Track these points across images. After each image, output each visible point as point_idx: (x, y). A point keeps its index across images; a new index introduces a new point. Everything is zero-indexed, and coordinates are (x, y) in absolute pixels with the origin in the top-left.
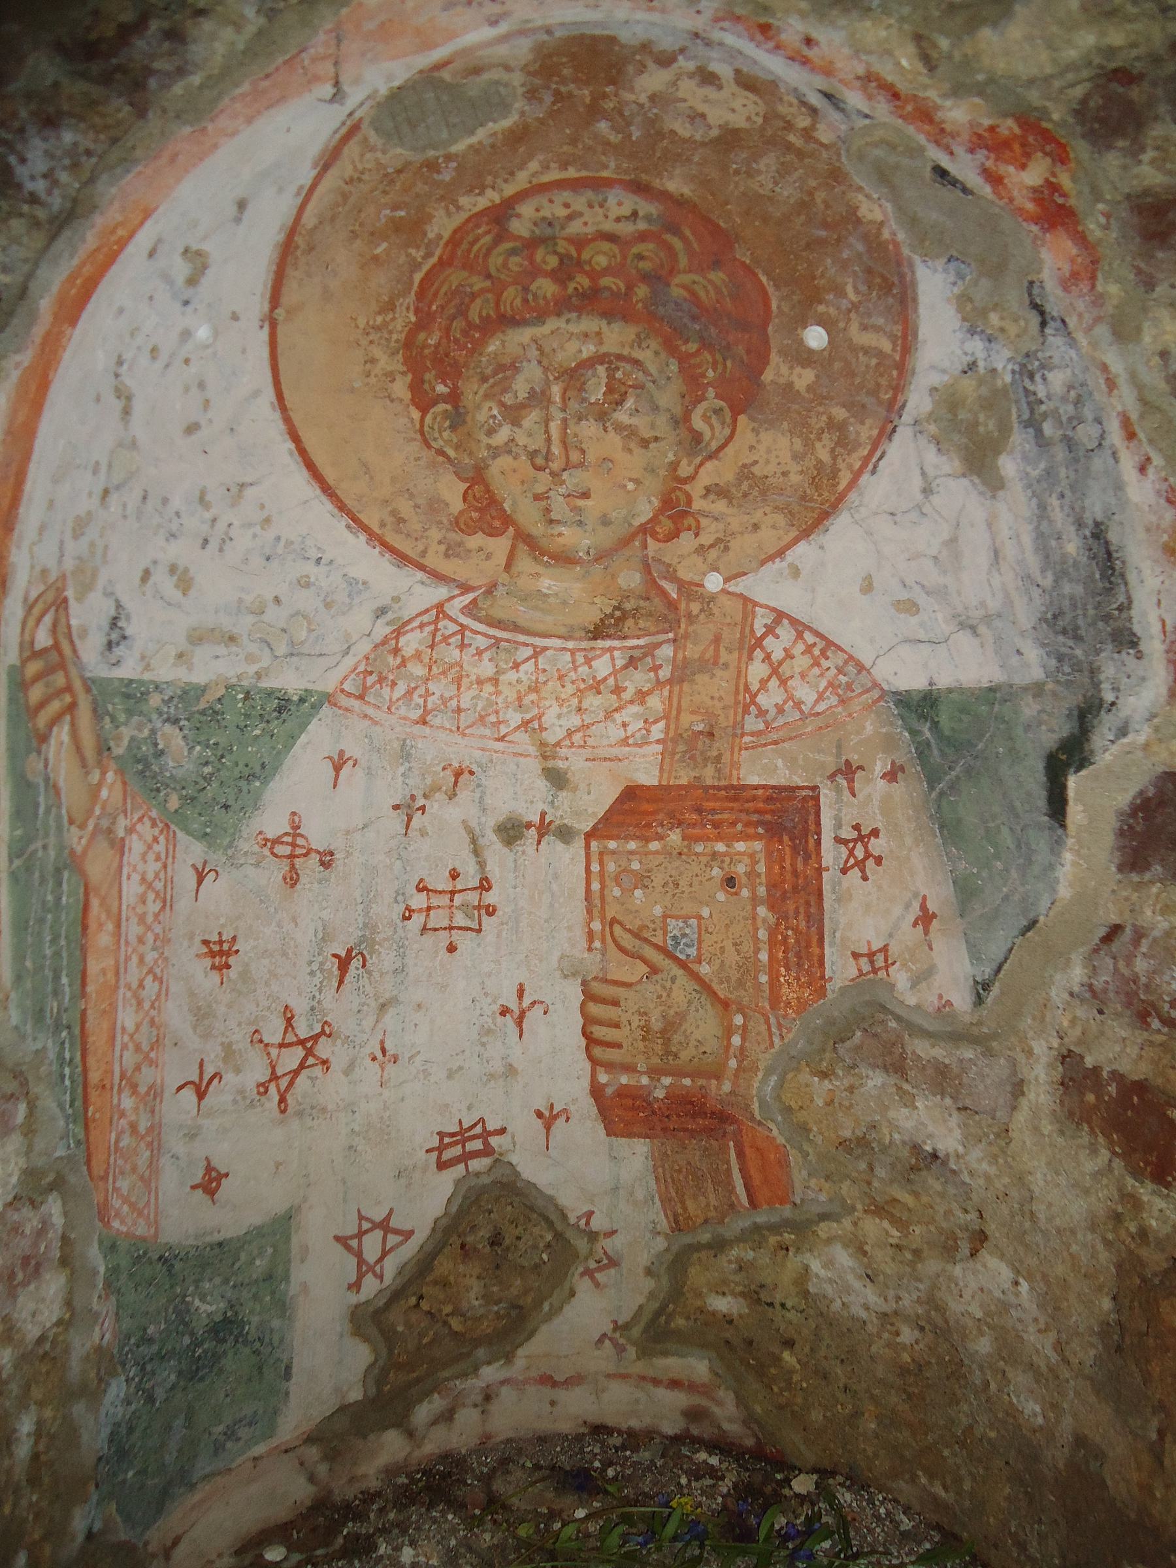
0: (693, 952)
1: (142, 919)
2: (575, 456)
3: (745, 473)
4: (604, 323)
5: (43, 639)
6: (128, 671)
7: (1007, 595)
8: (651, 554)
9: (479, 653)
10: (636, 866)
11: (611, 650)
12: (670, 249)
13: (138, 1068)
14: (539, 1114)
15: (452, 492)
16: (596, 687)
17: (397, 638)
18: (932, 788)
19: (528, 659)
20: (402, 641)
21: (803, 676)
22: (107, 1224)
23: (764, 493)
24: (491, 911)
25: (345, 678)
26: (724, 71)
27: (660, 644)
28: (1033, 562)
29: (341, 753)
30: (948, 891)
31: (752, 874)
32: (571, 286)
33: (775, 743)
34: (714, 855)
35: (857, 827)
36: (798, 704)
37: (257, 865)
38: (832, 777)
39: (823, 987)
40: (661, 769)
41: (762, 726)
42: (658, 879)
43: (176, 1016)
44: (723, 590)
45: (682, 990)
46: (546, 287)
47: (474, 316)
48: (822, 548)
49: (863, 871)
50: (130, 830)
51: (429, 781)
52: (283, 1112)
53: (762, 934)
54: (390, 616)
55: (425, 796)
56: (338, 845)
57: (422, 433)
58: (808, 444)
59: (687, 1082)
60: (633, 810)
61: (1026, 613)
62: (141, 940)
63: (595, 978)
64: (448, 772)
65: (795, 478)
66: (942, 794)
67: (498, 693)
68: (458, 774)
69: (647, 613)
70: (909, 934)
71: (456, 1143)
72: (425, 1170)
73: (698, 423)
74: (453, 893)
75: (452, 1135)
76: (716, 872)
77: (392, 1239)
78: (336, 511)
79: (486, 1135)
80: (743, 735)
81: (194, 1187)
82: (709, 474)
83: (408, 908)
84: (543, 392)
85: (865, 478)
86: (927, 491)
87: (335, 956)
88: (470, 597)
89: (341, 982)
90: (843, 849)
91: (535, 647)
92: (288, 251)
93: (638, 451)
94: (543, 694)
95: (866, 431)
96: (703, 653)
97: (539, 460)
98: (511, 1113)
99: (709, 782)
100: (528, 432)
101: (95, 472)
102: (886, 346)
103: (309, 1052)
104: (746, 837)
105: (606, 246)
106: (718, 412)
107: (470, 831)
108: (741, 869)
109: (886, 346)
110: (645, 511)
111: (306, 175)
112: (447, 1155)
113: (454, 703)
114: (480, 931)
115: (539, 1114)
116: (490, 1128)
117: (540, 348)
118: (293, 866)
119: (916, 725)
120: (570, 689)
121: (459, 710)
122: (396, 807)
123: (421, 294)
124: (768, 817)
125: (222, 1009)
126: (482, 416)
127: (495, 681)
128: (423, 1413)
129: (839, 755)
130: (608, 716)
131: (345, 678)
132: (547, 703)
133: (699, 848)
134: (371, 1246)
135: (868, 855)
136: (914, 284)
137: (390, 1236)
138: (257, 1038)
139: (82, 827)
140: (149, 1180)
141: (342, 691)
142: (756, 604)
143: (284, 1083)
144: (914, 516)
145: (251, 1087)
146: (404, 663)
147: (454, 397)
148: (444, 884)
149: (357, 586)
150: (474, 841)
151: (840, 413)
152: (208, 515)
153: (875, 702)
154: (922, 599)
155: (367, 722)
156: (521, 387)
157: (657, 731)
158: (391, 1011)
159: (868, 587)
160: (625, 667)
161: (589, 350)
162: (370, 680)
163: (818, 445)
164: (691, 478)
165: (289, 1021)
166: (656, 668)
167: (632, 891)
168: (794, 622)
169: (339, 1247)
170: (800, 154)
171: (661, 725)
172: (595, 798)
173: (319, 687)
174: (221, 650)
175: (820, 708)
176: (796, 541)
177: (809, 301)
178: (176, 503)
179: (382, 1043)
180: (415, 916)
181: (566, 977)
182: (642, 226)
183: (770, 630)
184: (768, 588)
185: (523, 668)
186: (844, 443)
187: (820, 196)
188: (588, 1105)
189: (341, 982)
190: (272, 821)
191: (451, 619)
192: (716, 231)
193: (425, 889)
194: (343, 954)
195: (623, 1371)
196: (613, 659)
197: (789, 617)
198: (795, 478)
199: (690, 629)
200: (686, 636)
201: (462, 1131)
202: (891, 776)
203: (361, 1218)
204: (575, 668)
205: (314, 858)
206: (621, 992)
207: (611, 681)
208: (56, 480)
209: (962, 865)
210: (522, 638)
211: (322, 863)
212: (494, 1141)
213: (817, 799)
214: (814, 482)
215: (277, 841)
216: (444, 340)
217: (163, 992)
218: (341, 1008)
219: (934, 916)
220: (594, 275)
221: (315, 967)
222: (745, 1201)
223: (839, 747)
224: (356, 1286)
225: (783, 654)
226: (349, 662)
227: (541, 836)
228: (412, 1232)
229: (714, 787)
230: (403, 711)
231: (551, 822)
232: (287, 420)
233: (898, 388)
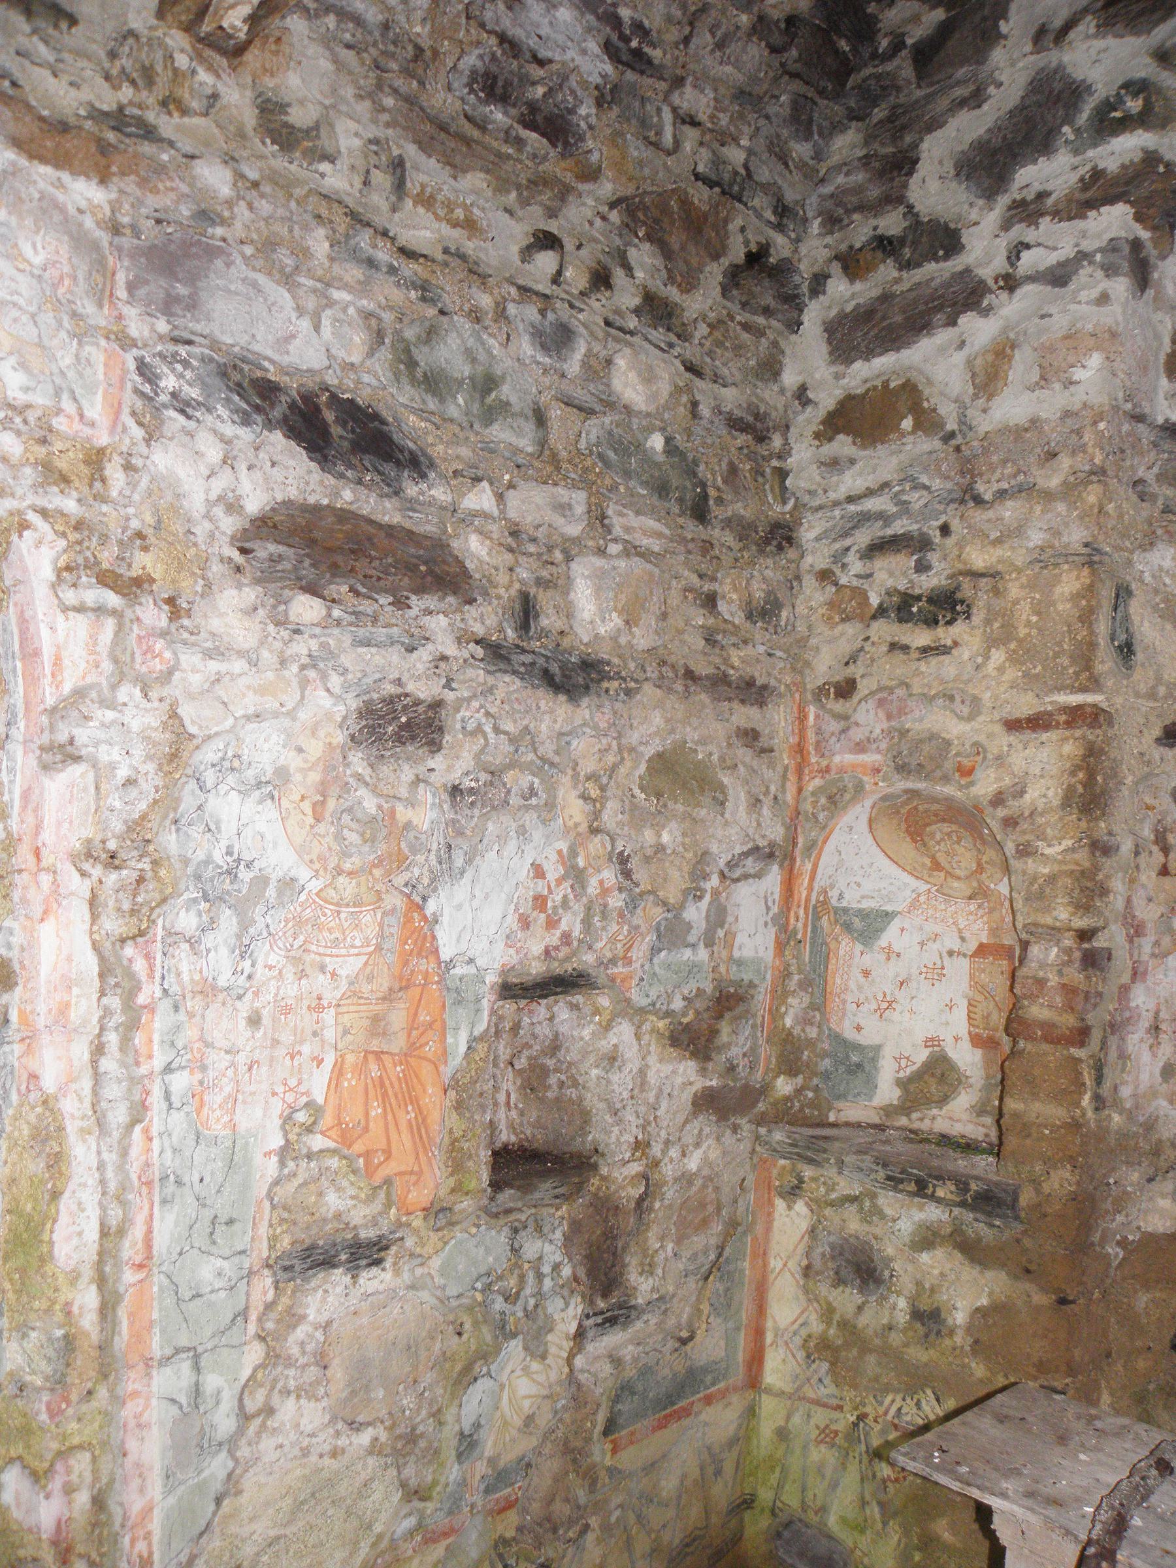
6: (844, 904)
15: (928, 862)
43: (852, 985)
60: (982, 950)
92: (870, 821)
97: (947, 853)
98: (947, 1036)
128: (914, 1116)
134: (903, 1063)
172: (972, 946)
188: (966, 1037)
190: (883, 942)
218: (901, 995)
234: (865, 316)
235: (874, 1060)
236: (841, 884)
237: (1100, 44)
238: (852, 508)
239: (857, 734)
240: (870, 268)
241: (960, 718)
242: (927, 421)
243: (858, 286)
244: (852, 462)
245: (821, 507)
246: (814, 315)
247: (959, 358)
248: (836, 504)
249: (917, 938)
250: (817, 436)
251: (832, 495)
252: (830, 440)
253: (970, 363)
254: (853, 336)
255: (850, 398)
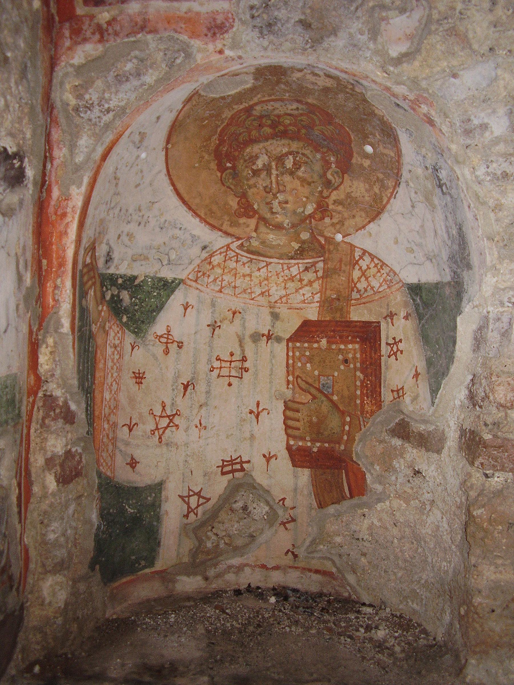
0: (330, 390)
1: (113, 361)
2: (281, 188)
3: (348, 196)
4: (291, 141)
5: (88, 260)
6: (112, 271)
7: (440, 248)
8: (313, 226)
9: (244, 264)
10: (307, 353)
11: (298, 264)
12: (313, 120)
13: (110, 415)
14: (264, 456)
15: (233, 203)
16: (292, 279)
17: (211, 258)
18: (420, 323)
19: (264, 267)
20: (213, 259)
21: (374, 276)
22: (99, 467)
23: (356, 203)
24: (247, 370)
25: (190, 274)
26: (321, 73)
27: (317, 262)
28: (445, 236)
29: (187, 303)
30: (424, 363)
31: (354, 358)
32: (277, 130)
33: (364, 303)
34: (340, 349)
35: (394, 339)
36: (372, 288)
37: (153, 345)
38: (385, 318)
39: (381, 405)
40: (319, 313)
41: (359, 297)
42: (317, 359)
43: (122, 398)
44: (342, 241)
45: (325, 407)
46: (268, 130)
47: (241, 139)
48: (379, 225)
49: (396, 356)
50: (110, 328)
51: (222, 316)
52: (160, 442)
53: (358, 383)
54: (208, 249)
55: (221, 322)
56: (185, 340)
57: (221, 180)
58: (371, 187)
59: (327, 445)
60: (306, 331)
61: (445, 255)
62: (112, 368)
63: (289, 400)
64: (230, 312)
65: (367, 198)
66: (423, 325)
67: (251, 280)
68: (234, 313)
70: (411, 381)
71: (229, 465)
72: (216, 474)
73: (329, 176)
74: (231, 362)
75: (227, 461)
76: (340, 357)
77: (201, 501)
78: (187, 210)
79: (241, 463)
80: (351, 300)
81: (127, 464)
82: (334, 196)
83: (212, 367)
84: (268, 165)
85: (392, 200)
86: (413, 207)
87: (182, 384)
88: (240, 242)
89: (184, 394)
90: (389, 347)
91: (267, 262)
93: (306, 186)
94: (270, 281)
95: (390, 183)
96: (335, 266)
99: (338, 319)
100: (262, 181)
101: (107, 204)
102: (392, 154)
103: (171, 421)
104: (351, 342)
105: (289, 117)
106: (337, 173)
107: (238, 336)
108: (350, 356)
109: (392, 154)
110: (310, 209)
111: (180, 107)
112: (226, 469)
113: (233, 284)
114: (242, 378)
115: (264, 456)
116: (243, 460)
117: (266, 150)
118: (167, 347)
119: (415, 298)
120: (281, 279)
121: (235, 287)
122: (208, 326)
123: (220, 135)
124: (360, 334)
125: (139, 399)
126: (245, 174)
127: (250, 276)
129: (388, 309)
130: (297, 291)
131: (190, 274)
132: (272, 285)
133: (334, 347)
134: (193, 501)
135: (398, 350)
136: (397, 135)
137: (201, 499)
138: (151, 412)
139: (96, 325)
140: (112, 457)
141: (188, 278)
142: (355, 247)
143: (161, 431)
144: (409, 215)
145: (148, 431)
146: (213, 268)
147: (234, 168)
148: (228, 358)
149: (194, 238)
150: (240, 341)
151: (381, 176)
152: (141, 214)
153: (401, 287)
154: (415, 248)
155: (198, 291)
156: (260, 163)
157: (317, 297)
158: (204, 408)
159: (396, 242)
160: (304, 271)
161: (285, 150)
162: (200, 274)
163: (375, 187)
164: (328, 197)
165: (164, 407)
166: (316, 272)
167: (306, 364)
168: (370, 255)
169: (180, 500)
170: (352, 95)
171: (319, 295)
172: (289, 326)
173: (180, 277)
174: (143, 263)
175: (380, 290)
176: (369, 222)
177: (365, 138)
178: (131, 211)
179: (200, 421)
180: (215, 370)
181: (277, 399)
182: (300, 112)
183: (361, 257)
184: (360, 240)
185: (261, 270)
186: (383, 187)
187: (361, 106)
188: (284, 454)
189: (184, 394)
190: (159, 328)
191: (233, 251)
192: (327, 114)
193: (219, 359)
194: (186, 383)
195: (296, 565)
196: (299, 267)
197: (369, 253)
198: (367, 198)
199: (330, 256)
200: (329, 259)
201: (231, 461)
202: (406, 318)
203: (189, 490)
204: (283, 271)
205: (175, 344)
206: (301, 406)
207: (298, 277)
208: (96, 209)
209: (429, 353)
210: (261, 258)
211: (178, 346)
212: (245, 466)
213: (379, 327)
214: (374, 200)
215: (161, 336)
216: (229, 149)
217: (118, 389)
219: (420, 374)
220: (285, 126)
221: (174, 387)
222: (348, 495)
223: (388, 305)
224: (187, 516)
225: (366, 267)
226: (191, 267)
227: (268, 340)
228: (210, 499)
229: (340, 321)
230: (213, 287)
231: (272, 335)
232: (171, 179)
233: (399, 169)
235: (155, 506)
236: (111, 235)
249: (206, 318)
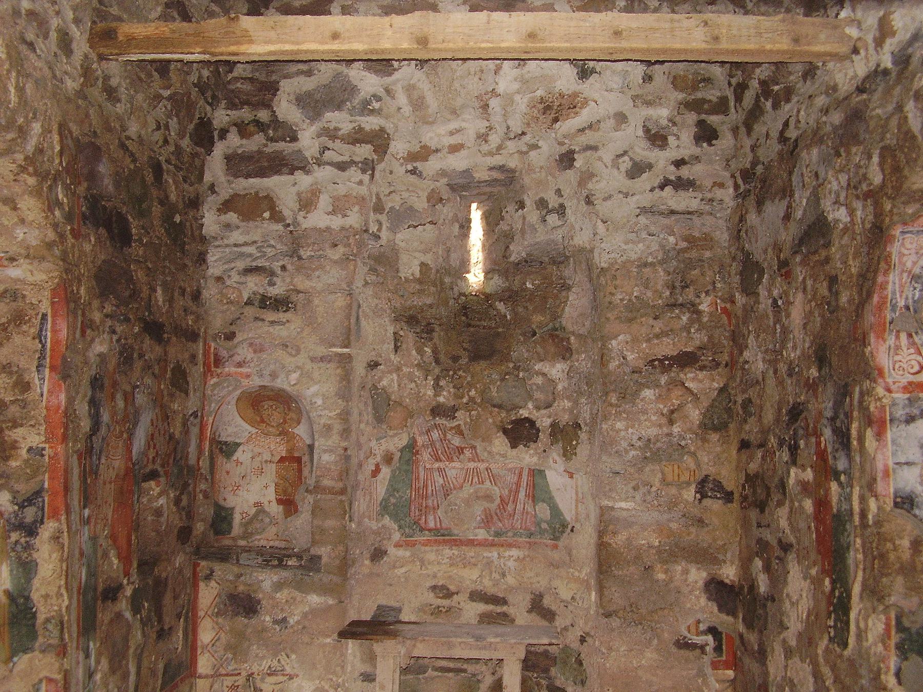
60: (282, 460)
69: (283, 433)
172: (278, 458)
184: (296, 431)
188: (274, 501)
190: (235, 458)
218: (242, 483)
234: (246, 158)
235: (232, 514)
236: (220, 429)
237: (364, 73)
238: (236, 249)
239: (237, 359)
240: (251, 135)
241: (291, 355)
242: (276, 217)
243: (244, 141)
244: (238, 227)
245: (219, 246)
246: (220, 149)
247: (294, 190)
248: (227, 246)
249: (250, 455)
250: (219, 210)
251: (226, 242)
252: (225, 213)
253: (299, 194)
254: (237, 164)
255: (236, 195)
